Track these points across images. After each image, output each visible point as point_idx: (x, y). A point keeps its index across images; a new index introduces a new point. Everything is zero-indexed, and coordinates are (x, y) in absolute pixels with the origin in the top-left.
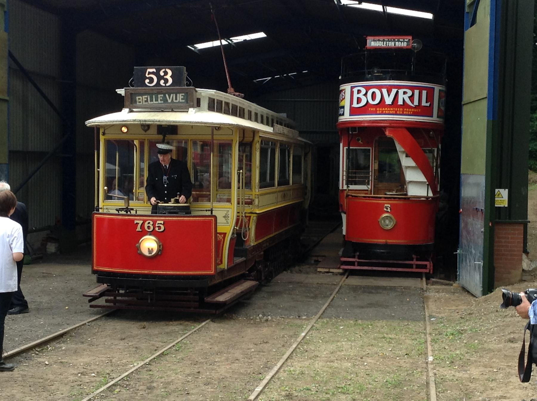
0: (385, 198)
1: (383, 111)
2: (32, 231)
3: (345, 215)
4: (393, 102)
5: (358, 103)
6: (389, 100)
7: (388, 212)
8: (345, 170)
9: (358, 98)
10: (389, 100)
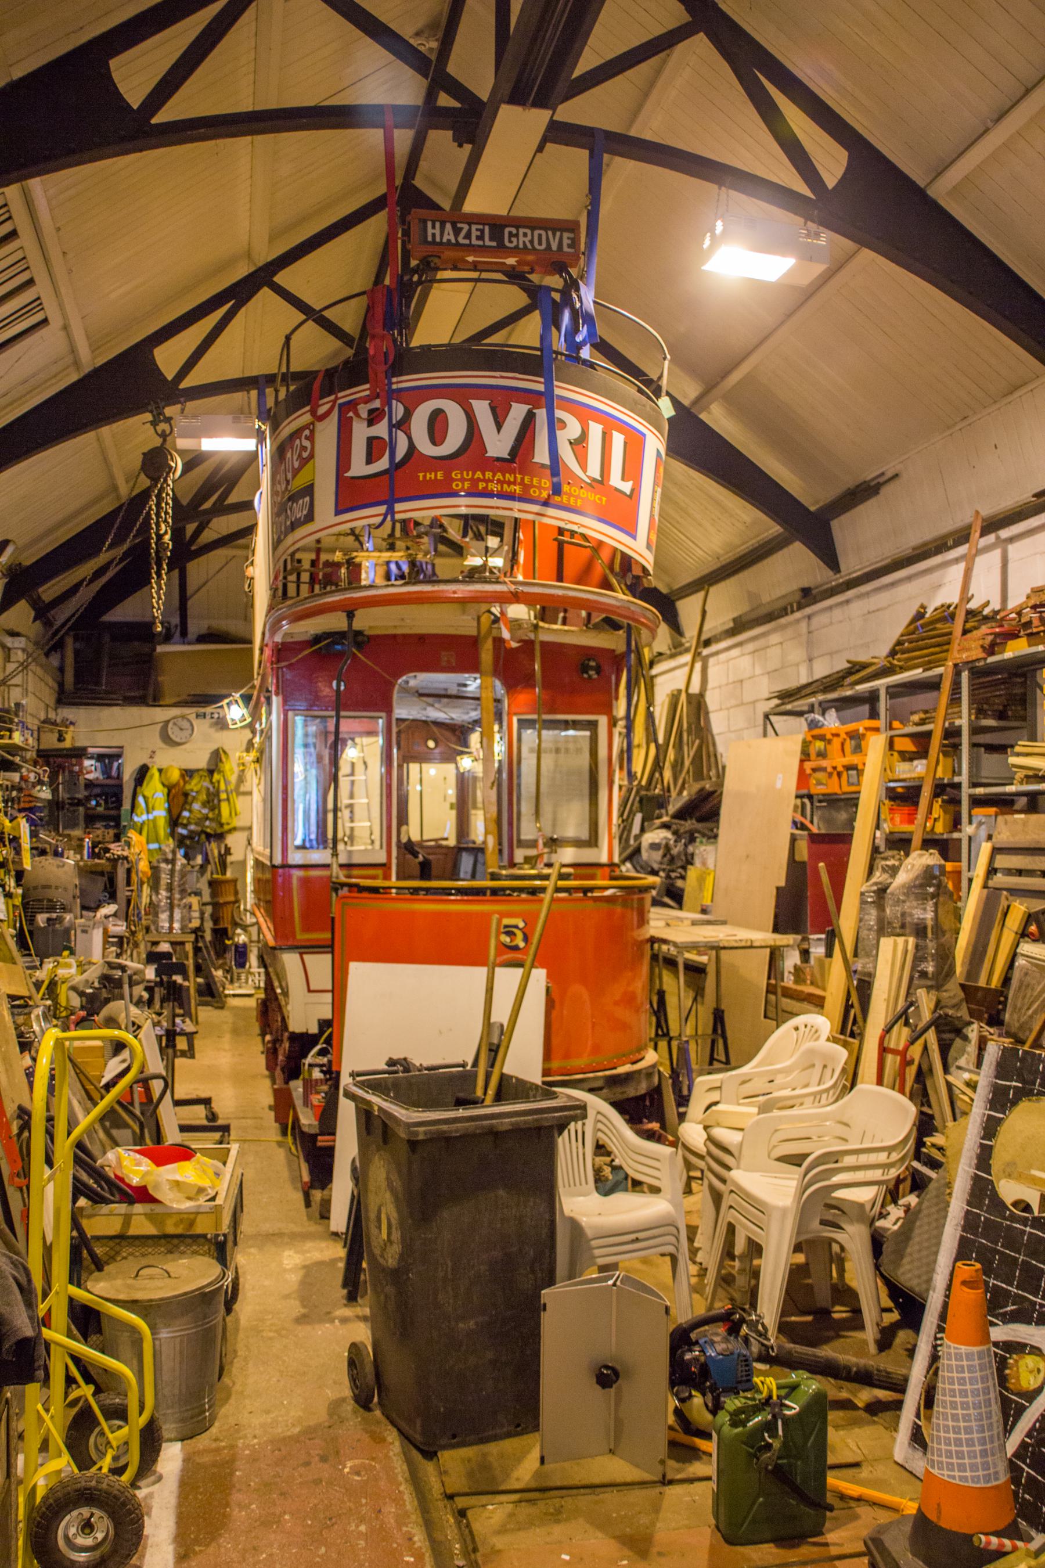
0: (495, 892)
1: (475, 482)
2: (243, 829)
3: (485, 404)
4: (514, 451)
5: (369, 461)
6: (498, 444)
7: (516, 948)
8: (445, 1127)
9: (371, 441)
10: (498, 444)
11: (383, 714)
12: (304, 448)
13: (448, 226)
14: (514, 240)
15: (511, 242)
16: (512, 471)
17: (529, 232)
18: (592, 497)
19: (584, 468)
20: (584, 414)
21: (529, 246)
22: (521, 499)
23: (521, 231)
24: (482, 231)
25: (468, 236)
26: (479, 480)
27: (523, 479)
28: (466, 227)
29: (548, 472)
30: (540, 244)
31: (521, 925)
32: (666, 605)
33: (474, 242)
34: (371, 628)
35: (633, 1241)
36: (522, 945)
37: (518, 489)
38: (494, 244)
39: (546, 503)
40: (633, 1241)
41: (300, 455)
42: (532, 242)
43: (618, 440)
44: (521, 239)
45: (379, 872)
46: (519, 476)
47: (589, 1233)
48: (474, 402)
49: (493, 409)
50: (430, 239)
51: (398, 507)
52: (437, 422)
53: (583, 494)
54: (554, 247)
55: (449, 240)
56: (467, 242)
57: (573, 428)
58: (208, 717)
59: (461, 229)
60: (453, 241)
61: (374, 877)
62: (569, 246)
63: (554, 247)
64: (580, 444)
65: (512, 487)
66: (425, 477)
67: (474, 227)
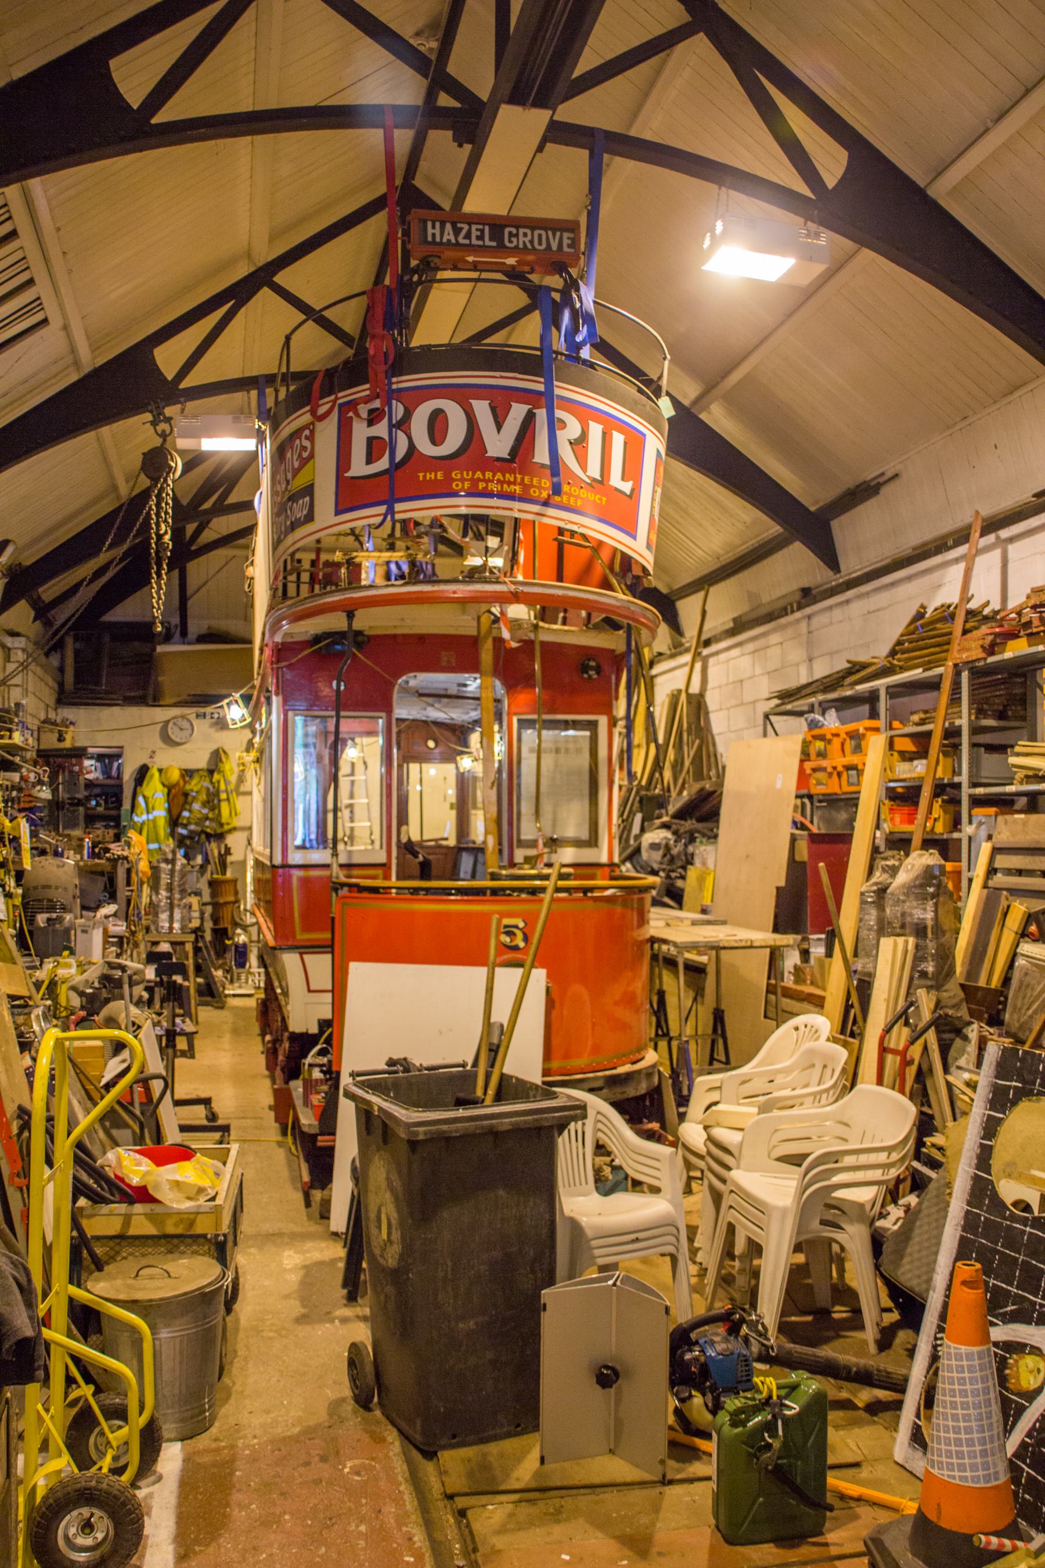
0: (495, 892)
1: (475, 482)
2: (243, 829)
3: (485, 404)
4: (514, 451)
5: (369, 461)
6: (498, 444)
7: (516, 948)
9: (371, 441)
10: (498, 444)
11: (383, 714)
12: (304, 448)
13: (448, 226)
14: (514, 240)
15: (511, 242)
16: (512, 471)
17: (529, 232)
18: (592, 497)
19: (584, 468)
20: (584, 414)
21: (529, 246)
22: (521, 499)
23: (521, 231)
24: (482, 231)
25: (468, 236)
26: (479, 480)
27: (523, 479)
28: (466, 227)
29: (548, 472)
30: (540, 244)
31: (521, 925)
32: (666, 605)
33: (474, 242)
34: (371, 628)
35: (633, 1241)
36: (522, 945)
37: (518, 489)
38: (494, 244)
39: (546, 503)
40: (633, 1241)
41: (300, 455)
42: (532, 242)
43: (618, 440)
44: (521, 239)
45: (379, 872)
46: (519, 476)
47: (589, 1233)
48: (474, 402)
49: (493, 409)
50: (430, 239)
51: (398, 507)
52: (437, 422)
53: (583, 494)
54: (554, 247)
55: (449, 240)
56: (467, 242)
57: (573, 428)
58: (208, 717)
59: (461, 229)
60: (453, 241)
61: (374, 877)
62: (569, 246)
63: (554, 247)
64: (580, 444)
65: (512, 487)
66: (425, 477)
67: (474, 227)
